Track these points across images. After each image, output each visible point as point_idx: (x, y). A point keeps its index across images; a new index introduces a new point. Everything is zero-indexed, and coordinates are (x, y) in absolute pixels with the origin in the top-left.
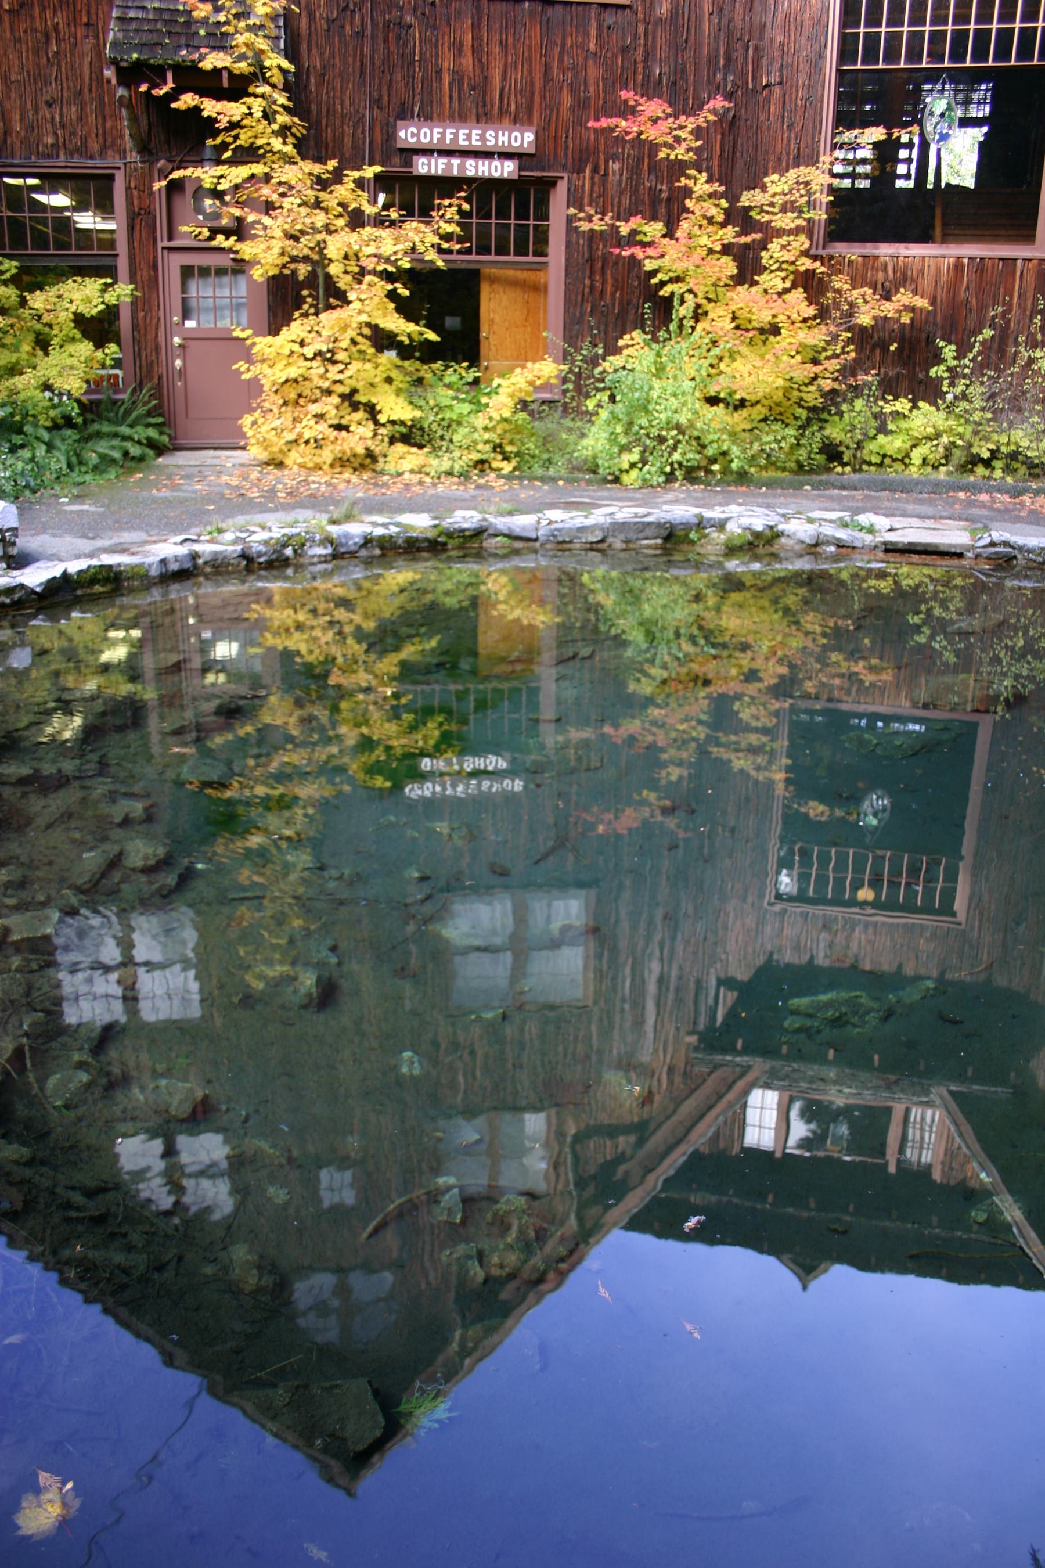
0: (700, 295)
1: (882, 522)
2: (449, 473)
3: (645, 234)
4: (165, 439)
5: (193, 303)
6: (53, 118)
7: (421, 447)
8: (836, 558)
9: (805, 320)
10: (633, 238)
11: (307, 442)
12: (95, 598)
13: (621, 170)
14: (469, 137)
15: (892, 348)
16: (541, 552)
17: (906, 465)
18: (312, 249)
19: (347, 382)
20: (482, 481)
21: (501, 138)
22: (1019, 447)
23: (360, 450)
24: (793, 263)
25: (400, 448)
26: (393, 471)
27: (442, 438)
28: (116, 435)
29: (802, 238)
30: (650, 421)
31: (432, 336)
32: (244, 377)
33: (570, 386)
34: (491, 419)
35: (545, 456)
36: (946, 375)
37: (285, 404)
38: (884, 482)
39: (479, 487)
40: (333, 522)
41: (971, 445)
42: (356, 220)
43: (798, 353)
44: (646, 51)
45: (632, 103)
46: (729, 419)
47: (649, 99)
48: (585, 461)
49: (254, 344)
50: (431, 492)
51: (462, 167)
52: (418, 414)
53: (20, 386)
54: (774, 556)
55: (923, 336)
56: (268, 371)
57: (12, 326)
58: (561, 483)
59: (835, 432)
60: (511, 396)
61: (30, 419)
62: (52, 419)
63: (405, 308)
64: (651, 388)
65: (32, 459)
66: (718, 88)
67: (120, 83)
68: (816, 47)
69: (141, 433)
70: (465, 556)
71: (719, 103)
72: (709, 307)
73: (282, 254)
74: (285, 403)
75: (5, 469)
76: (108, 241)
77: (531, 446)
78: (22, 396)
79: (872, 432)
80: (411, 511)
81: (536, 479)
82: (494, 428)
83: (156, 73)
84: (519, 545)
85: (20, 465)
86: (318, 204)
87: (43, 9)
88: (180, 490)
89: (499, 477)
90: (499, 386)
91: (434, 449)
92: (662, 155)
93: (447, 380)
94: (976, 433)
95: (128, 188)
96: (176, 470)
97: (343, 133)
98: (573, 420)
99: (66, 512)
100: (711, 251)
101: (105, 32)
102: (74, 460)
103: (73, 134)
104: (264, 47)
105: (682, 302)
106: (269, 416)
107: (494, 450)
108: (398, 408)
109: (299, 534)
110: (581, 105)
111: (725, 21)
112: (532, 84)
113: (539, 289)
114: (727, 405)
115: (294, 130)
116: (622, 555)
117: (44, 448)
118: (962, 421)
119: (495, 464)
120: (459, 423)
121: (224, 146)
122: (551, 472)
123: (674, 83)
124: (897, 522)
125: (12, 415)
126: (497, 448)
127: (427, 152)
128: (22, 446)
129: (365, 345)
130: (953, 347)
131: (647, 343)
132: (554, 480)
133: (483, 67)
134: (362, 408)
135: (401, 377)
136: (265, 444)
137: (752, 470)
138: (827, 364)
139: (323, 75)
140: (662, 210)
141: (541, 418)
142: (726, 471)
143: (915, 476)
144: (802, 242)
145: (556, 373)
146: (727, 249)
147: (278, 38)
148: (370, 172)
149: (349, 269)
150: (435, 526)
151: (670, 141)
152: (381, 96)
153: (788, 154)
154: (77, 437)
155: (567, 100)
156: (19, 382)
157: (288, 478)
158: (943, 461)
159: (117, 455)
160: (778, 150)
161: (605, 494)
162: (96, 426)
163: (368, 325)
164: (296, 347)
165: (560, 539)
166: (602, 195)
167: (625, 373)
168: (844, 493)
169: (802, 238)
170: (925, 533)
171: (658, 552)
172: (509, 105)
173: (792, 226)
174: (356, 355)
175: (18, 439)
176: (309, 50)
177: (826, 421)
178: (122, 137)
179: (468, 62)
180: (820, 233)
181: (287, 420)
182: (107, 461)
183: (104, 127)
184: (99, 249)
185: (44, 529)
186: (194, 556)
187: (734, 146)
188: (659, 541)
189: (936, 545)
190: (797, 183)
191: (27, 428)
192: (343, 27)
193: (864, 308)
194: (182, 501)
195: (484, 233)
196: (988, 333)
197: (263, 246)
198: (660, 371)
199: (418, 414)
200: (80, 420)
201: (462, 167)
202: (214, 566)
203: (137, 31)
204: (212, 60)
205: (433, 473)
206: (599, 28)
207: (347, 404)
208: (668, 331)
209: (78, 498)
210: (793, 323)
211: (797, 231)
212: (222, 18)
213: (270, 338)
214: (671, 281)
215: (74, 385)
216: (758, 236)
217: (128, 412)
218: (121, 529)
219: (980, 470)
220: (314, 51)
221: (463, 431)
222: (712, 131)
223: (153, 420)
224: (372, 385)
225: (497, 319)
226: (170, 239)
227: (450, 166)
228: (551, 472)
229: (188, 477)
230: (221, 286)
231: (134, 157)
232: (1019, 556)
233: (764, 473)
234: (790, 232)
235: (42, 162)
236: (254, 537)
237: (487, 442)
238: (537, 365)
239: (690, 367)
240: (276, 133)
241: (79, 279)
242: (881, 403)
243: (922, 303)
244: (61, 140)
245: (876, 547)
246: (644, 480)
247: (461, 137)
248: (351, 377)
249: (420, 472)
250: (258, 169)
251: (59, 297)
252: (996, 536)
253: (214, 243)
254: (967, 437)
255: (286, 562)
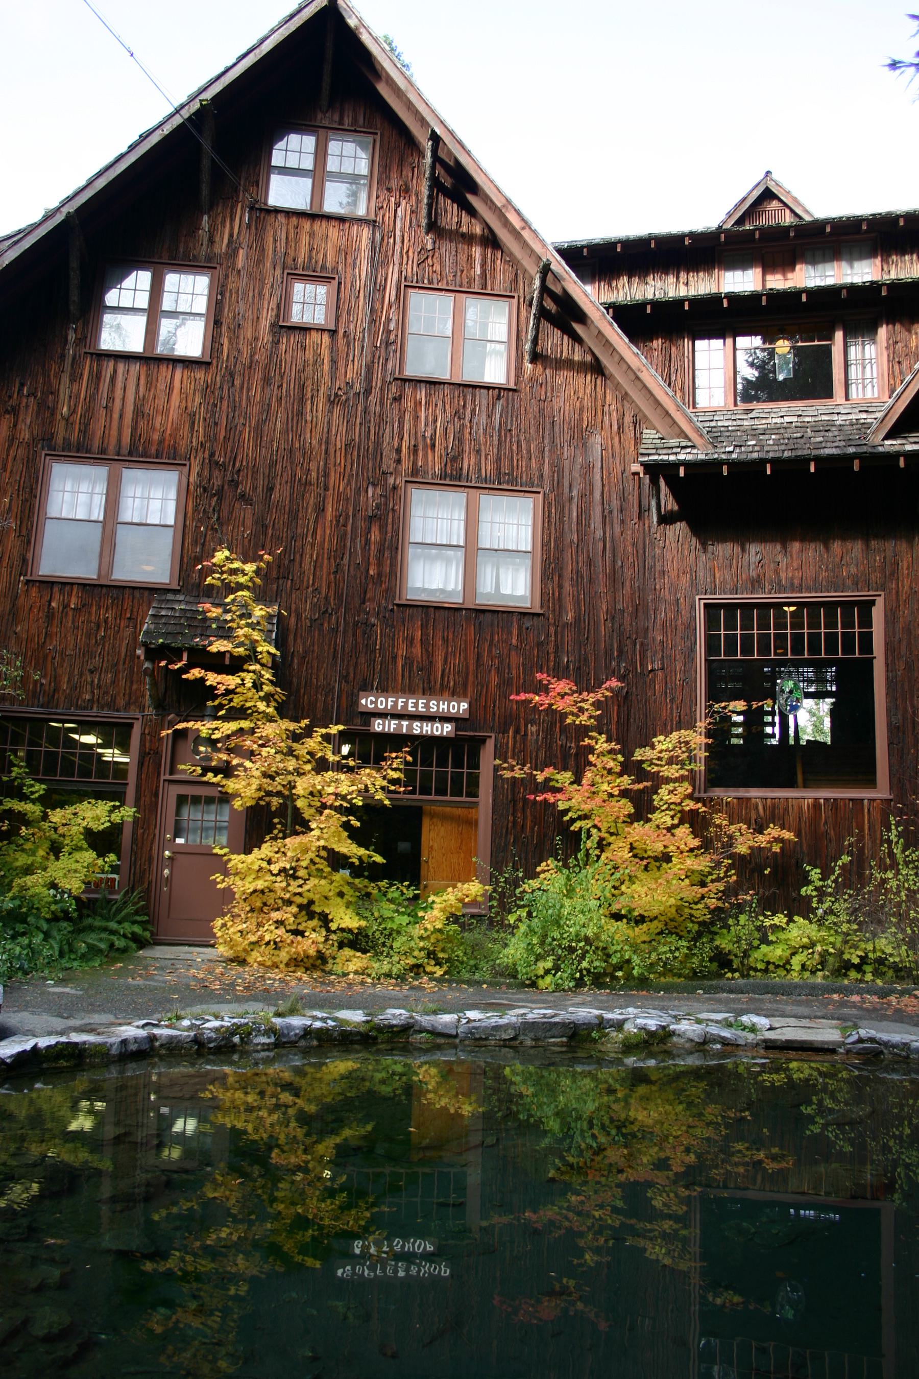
0: (603, 830)
1: (762, 1022)
2: (388, 975)
3: (557, 781)
4: (147, 934)
5: (185, 824)
6: (93, 681)
7: (364, 952)
8: (722, 1055)
9: (691, 850)
10: (548, 786)
11: (268, 943)
12: (59, 1072)
13: (538, 731)
14: (416, 705)
15: (766, 872)
16: (460, 1048)
17: (788, 971)
18: (284, 786)
19: (306, 894)
20: (416, 983)
21: (441, 706)
22: (884, 953)
23: (312, 952)
24: (680, 804)
25: (347, 952)
26: (340, 972)
27: (384, 944)
28: (105, 929)
29: (686, 784)
30: (562, 934)
31: (379, 859)
32: (219, 886)
33: (495, 903)
34: (426, 929)
35: (472, 962)
36: (814, 893)
37: (252, 910)
38: (767, 985)
39: (412, 988)
40: (278, 1015)
41: (843, 953)
42: (322, 766)
43: (687, 877)
44: (556, 646)
45: (545, 682)
46: (630, 932)
47: (559, 680)
48: (507, 967)
49: (230, 860)
50: (371, 991)
51: (410, 727)
52: (363, 923)
53: (29, 884)
54: (668, 1054)
55: (793, 861)
56: (239, 883)
57: (33, 834)
58: (485, 986)
59: (724, 943)
60: (443, 910)
61: (35, 911)
62: (53, 913)
63: (355, 835)
64: (562, 906)
65: (29, 946)
66: (614, 672)
67: (147, 659)
68: (688, 644)
69: (128, 928)
70: (392, 1050)
71: (614, 683)
72: (612, 839)
73: (259, 789)
74: (252, 910)
75: (4, 953)
76: (119, 770)
77: (460, 953)
78: (30, 892)
79: (756, 943)
80: (349, 1008)
81: (464, 982)
82: (428, 937)
83: (173, 653)
84: (441, 1041)
85: (18, 949)
86: (290, 752)
87: (99, 608)
88: (153, 980)
89: (431, 980)
90: (433, 902)
91: (376, 954)
92: (568, 721)
93: (390, 896)
94: (846, 942)
95: (143, 734)
96: (152, 962)
97: (316, 700)
98: (498, 932)
99: (49, 993)
100: (611, 795)
101: (142, 625)
102: (66, 948)
103: (106, 693)
104: (258, 638)
105: (589, 836)
106: (237, 920)
107: (429, 957)
108: (347, 919)
109: (247, 1024)
110: (506, 684)
111: (616, 626)
112: (467, 668)
113: (472, 824)
114: (629, 920)
115: (276, 697)
116: (532, 1051)
117: (41, 936)
118: (832, 932)
119: (429, 969)
120: (399, 933)
121: (221, 707)
122: (477, 976)
123: (579, 668)
124: (777, 1022)
125: (20, 907)
126: (431, 955)
127: (383, 715)
128: (23, 934)
129: (323, 865)
130: (818, 871)
131: (559, 870)
132: (479, 983)
133: (429, 654)
134: (317, 917)
135: (351, 892)
136: (230, 943)
137: (652, 976)
138: (713, 887)
139: (304, 657)
140: (572, 762)
141: (471, 930)
142: (629, 977)
143: (796, 980)
144: (686, 788)
145: (481, 892)
146: (624, 793)
147: (271, 631)
148: (334, 729)
149: (313, 803)
150: (367, 1022)
151: (575, 711)
152: (348, 674)
153: (672, 721)
154: (70, 929)
155: (494, 680)
156: (29, 880)
157: (247, 974)
158: (819, 967)
159: (103, 946)
160: (663, 718)
161: (522, 996)
162: (89, 921)
163: (324, 848)
164: (264, 864)
165: (477, 1036)
166: (523, 750)
167: (540, 893)
168: (732, 996)
169: (686, 784)
170: (800, 1031)
171: (564, 1049)
172: (449, 682)
173: (677, 775)
174: (315, 873)
175: (20, 928)
176: (295, 640)
177: (716, 933)
178: (143, 696)
179: (417, 650)
180: (701, 780)
181: (251, 925)
182: (94, 951)
183: (131, 688)
184: (114, 778)
185: (25, 1007)
186: (152, 1038)
187: (628, 715)
188: (564, 1039)
189: (811, 1042)
190: (680, 742)
191: (31, 919)
192: (322, 625)
193: (741, 839)
194: (152, 990)
195: (426, 776)
196: (846, 859)
197: (243, 783)
198: (570, 892)
199: (363, 923)
200: (75, 915)
201: (410, 727)
202: (168, 1049)
203: (165, 624)
204: (219, 646)
205: (374, 975)
206: (520, 629)
207: (304, 913)
208: (576, 859)
209: (61, 982)
210: (682, 852)
211: (681, 779)
212: (228, 617)
213: (243, 856)
214: (580, 818)
215: (75, 885)
216: (648, 784)
217: (119, 910)
218: (94, 1011)
219: (853, 974)
220: (299, 641)
221: (402, 939)
222: (610, 703)
223: (139, 918)
224: (326, 898)
225: (436, 846)
226: (171, 774)
227: (400, 726)
228: (477, 976)
229: (162, 968)
230: (208, 813)
231: (150, 711)
232: (885, 1051)
233: (662, 979)
234: (676, 780)
235: (79, 712)
236: (207, 1025)
237: (421, 949)
238: (466, 886)
239: (596, 888)
240: (262, 699)
241: (93, 801)
242: (761, 918)
243: (787, 835)
244: (96, 697)
245: (757, 1044)
246: (557, 985)
247: (410, 705)
248: (309, 891)
249: (363, 974)
250: (245, 724)
251: (75, 814)
252: (863, 1033)
253: (205, 779)
254: (838, 945)
255: (233, 1048)
